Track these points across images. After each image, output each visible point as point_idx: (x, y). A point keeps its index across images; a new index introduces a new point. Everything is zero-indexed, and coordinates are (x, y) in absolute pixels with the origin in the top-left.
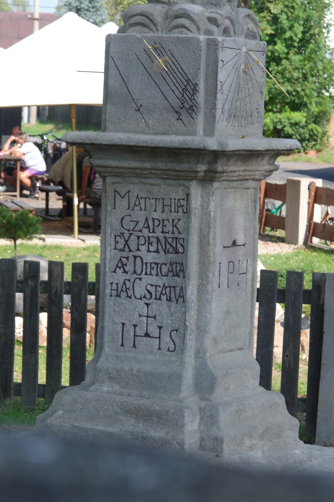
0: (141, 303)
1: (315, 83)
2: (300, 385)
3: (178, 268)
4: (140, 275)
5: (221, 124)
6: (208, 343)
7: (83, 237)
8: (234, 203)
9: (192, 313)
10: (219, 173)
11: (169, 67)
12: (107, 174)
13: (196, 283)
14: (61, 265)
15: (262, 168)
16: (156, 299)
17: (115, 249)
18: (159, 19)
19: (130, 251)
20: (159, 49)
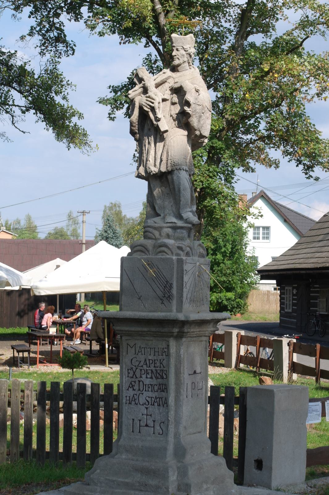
0: (143, 408)
1: (239, 276)
2: (234, 450)
3: (164, 387)
4: (142, 391)
5: (186, 306)
6: (181, 429)
7: (111, 366)
8: (194, 349)
9: (172, 412)
10: (186, 333)
11: (156, 274)
12: (123, 335)
13: (174, 395)
14: (98, 385)
15: (209, 330)
16: (151, 405)
17: (128, 377)
18: (150, 248)
19: (136, 378)
20: (151, 265)
